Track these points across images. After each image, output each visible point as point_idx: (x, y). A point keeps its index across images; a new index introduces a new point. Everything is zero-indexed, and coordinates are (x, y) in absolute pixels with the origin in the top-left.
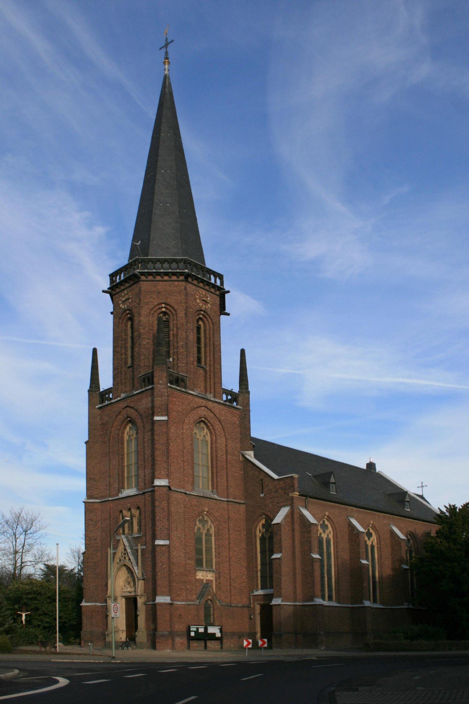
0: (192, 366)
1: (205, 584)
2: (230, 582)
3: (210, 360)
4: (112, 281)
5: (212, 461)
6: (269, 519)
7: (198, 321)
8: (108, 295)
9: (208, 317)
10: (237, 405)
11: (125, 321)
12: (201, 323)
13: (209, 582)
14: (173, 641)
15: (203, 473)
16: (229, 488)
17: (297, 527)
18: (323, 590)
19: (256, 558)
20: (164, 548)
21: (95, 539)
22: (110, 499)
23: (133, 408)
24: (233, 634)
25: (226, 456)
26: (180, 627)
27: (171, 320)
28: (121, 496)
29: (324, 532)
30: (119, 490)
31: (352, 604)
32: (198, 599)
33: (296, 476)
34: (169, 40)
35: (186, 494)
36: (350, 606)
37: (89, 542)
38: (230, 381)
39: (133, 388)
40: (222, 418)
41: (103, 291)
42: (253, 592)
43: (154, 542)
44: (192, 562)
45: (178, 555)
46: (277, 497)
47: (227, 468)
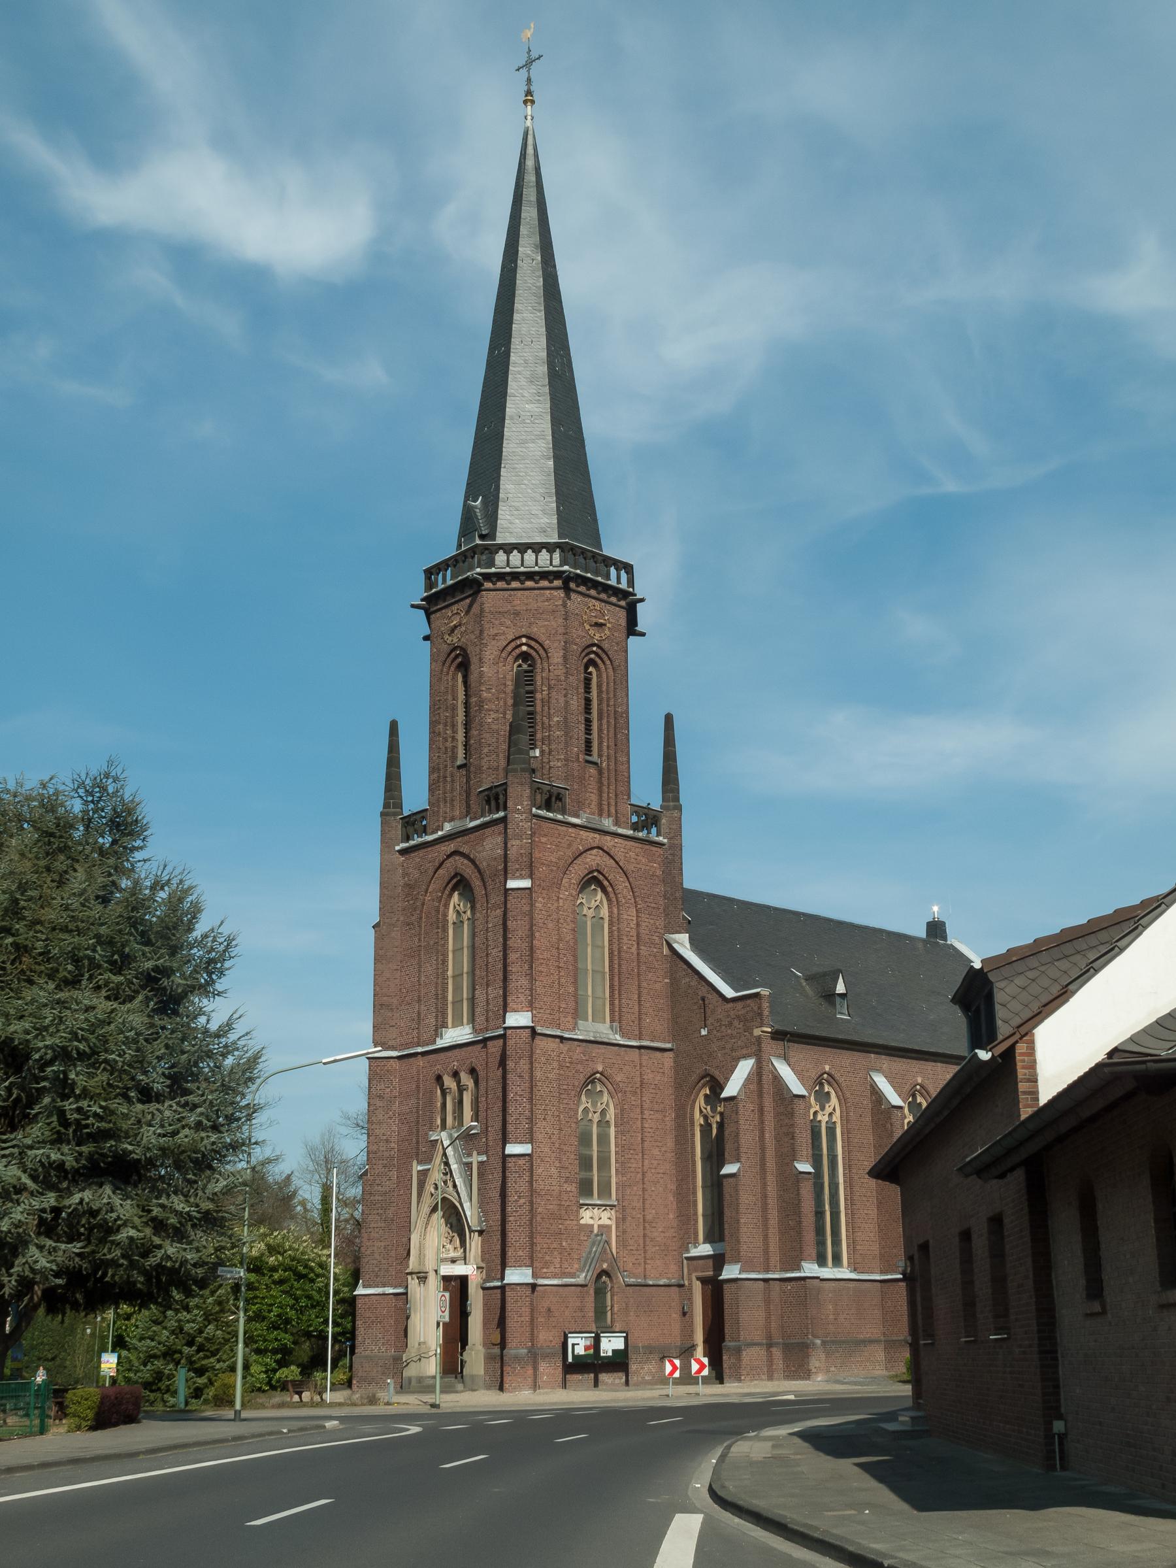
0: (576, 764)
1: (597, 1235)
2: (644, 1228)
3: (608, 747)
4: (430, 585)
5: (611, 961)
6: (717, 1086)
7: (586, 667)
8: (421, 614)
9: (604, 656)
10: (658, 834)
11: (452, 669)
12: (591, 669)
13: (604, 1229)
14: (535, 1369)
15: (595, 989)
16: (644, 1017)
17: (768, 1103)
18: (821, 1243)
19: (694, 1171)
20: (521, 1162)
21: (387, 1141)
22: (420, 1050)
23: (466, 856)
24: (650, 1350)
25: (638, 948)
26: (547, 1337)
27: (539, 670)
28: (441, 1043)
29: (823, 1108)
30: (436, 1030)
31: (882, 1272)
32: (583, 1271)
33: (765, 992)
34: (534, 55)
35: (562, 1039)
36: (878, 1277)
37: (374, 1148)
38: (646, 789)
39: (468, 813)
40: (630, 868)
41: (413, 606)
42: (688, 1251)
43: (504, 1149)
44: (572, 1188)
45: (549, 1175)
46: (732, 1037)
47: (639, 975)
